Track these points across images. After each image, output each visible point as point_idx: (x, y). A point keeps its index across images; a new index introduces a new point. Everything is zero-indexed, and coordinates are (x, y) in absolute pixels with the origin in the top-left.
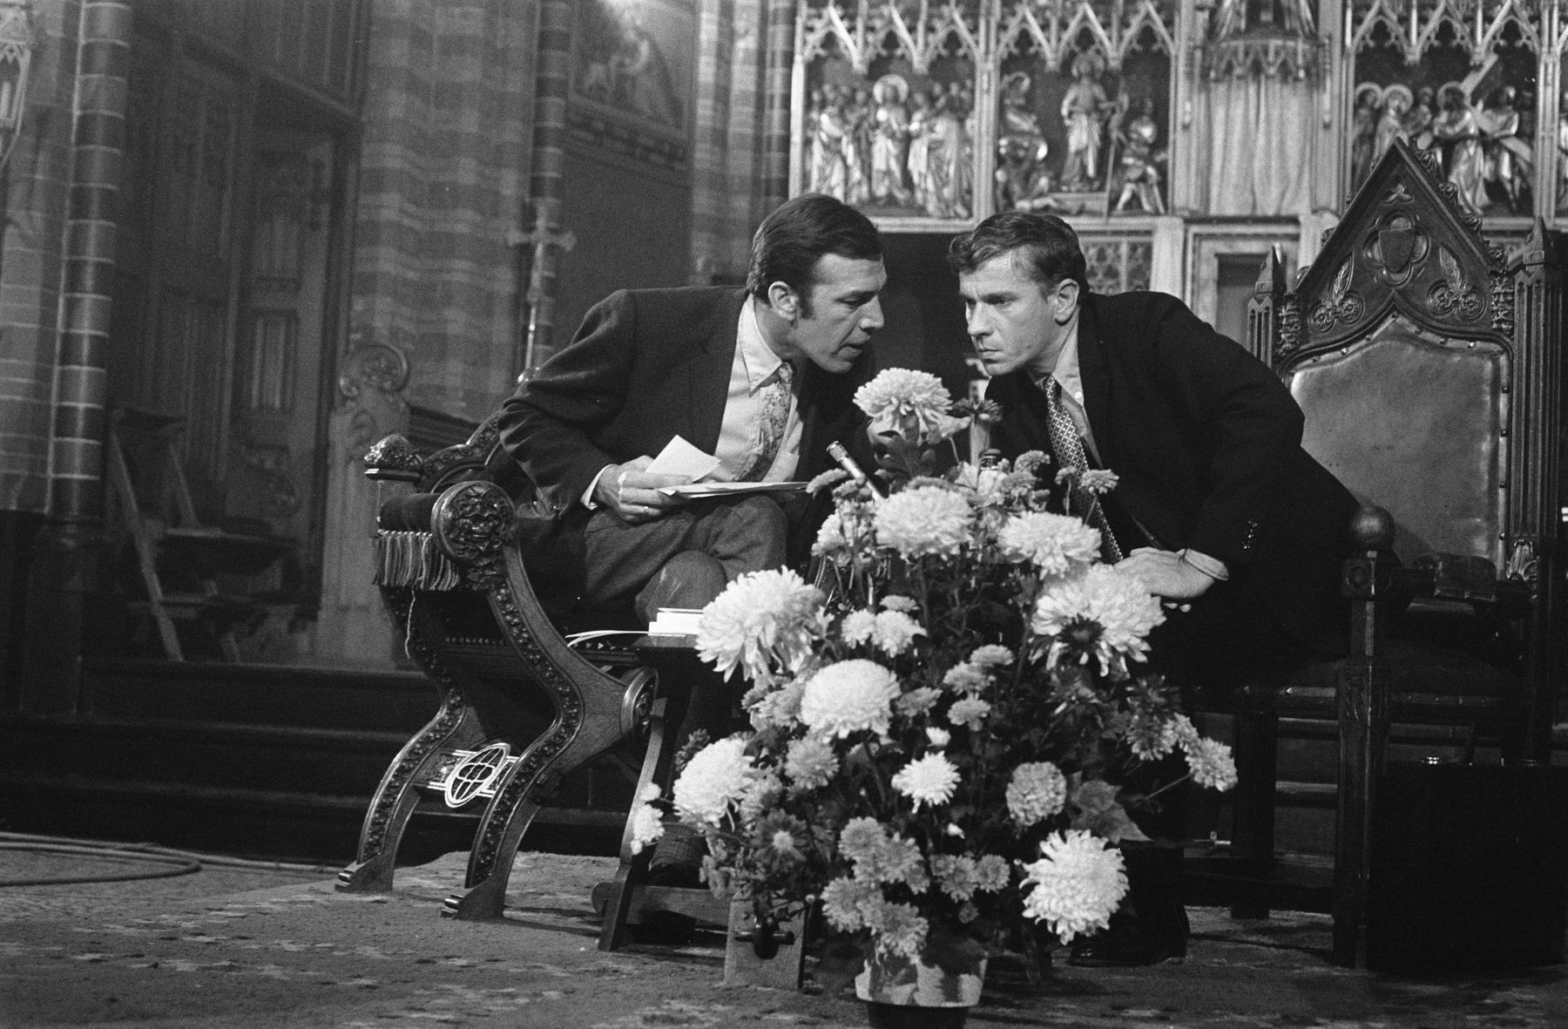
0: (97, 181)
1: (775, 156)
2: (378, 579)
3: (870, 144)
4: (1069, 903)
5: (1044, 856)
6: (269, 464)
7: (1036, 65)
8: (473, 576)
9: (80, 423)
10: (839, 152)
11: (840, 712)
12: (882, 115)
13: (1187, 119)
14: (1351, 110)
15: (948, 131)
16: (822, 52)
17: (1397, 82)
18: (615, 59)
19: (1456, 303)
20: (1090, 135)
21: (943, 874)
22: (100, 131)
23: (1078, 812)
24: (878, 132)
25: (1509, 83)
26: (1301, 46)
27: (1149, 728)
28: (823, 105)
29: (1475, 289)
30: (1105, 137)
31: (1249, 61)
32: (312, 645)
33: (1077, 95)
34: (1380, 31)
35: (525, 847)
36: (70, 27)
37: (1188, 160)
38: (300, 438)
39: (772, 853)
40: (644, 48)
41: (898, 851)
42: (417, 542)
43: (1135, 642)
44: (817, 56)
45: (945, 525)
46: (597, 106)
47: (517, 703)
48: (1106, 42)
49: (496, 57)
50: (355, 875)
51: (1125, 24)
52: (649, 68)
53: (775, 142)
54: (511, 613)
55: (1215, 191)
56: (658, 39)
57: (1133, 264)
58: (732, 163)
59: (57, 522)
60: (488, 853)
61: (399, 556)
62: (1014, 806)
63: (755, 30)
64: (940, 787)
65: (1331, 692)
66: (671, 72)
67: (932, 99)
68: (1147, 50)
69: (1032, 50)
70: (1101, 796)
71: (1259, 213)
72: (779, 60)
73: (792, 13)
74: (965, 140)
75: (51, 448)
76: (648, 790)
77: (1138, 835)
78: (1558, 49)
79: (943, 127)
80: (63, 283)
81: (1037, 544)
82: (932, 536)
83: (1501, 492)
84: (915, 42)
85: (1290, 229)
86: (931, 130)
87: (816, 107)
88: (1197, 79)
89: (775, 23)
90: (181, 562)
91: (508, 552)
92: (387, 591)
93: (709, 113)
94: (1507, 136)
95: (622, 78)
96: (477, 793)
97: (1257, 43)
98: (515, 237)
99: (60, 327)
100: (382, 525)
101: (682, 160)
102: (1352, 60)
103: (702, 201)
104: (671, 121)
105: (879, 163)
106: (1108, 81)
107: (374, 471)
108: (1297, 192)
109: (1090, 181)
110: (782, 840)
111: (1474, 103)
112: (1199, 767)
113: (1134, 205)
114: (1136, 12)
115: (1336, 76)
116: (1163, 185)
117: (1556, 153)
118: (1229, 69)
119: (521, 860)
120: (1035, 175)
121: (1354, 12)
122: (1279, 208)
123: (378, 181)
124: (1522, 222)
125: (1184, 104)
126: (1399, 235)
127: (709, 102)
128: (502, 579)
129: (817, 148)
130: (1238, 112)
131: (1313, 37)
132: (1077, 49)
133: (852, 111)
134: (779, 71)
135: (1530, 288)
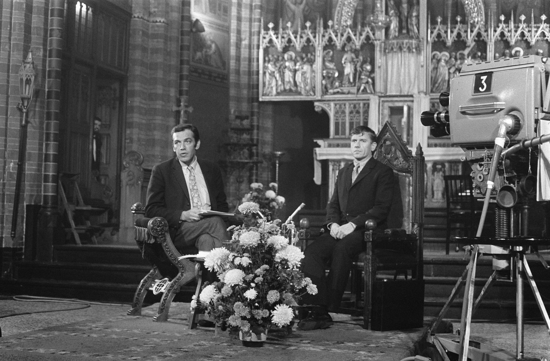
0: (53, 110)
2: (136, 239)
3: (284, 73)
7: (334, 47)
8: (158, 240)
9: (51, 179)
10: (274, 76)
13: (380, 65)
16: (268, 45)
17: (445, 51)
18: (204, 50)
20: (351, 69)
22: (53, 95)
23: (284, 300)
24: (286, 69)
25: (480, 51)
28: (269, 61)
30: (356, 70)
31: (398, 46)
32: (118, 239)
33: (347, 56)
34: (439, 36)
35: (175, 301)
36: (44, 66)
38: (112, 172)
39: (218, 310)
40: (213, 46)
41: (244, 309)
42: (144, 230)
43: (297, 262)
44: (267, 46)
46: (199, 65)
47: (169, 270)
48: (355, 40)
49: (168, 53)
51: (361, 35)
52: (214, 53)
53: (255, 73)
56: (217, 43)
57: (365, 109)
59: (45, 207)
61: (140, 233)
62: (268, 299)
63: (248, 38)
65: (363, 264)
66: (222, 54)
67: (302, 59)
68: (368, 42)
69: (333, 43)
71: (402, 94)
72: (255, 47)
73: (259, 33)
74: (313, 71)
75: (43, 186)
78: (493, 41)
79: (306, 67)
80: (44, 139)
83: (411, 211)
85: (411, 99)
86: (302, 68)
89: (254, 35)
90: (79, 217)
91: (166, 234)
92: (138, 241)
93: (234, 64)
95: (206, 56)
96: (161, 291)
97: (400, 41)
98: (175, 108)
100: (136, 225)
101: (226, 79)
102: (431, 44)
103: (232, 92)
104: (222, 68)
105: (287, 79)
106: (356, 52)
107: (134, 212)
108: (414, 85)
109: (351, 83)
110: (220, 307)
111: (468, 57)
114: (364, 31)
116: (374, 84)
118: (392, 49)
120: (334, 82)
122: (408, 92)
123: (133, 94)
125: (379, 59)
126: (388, 145)
127: (234, 61)
129: (267, 75)
130: (395, 62)
132: (346, 42)
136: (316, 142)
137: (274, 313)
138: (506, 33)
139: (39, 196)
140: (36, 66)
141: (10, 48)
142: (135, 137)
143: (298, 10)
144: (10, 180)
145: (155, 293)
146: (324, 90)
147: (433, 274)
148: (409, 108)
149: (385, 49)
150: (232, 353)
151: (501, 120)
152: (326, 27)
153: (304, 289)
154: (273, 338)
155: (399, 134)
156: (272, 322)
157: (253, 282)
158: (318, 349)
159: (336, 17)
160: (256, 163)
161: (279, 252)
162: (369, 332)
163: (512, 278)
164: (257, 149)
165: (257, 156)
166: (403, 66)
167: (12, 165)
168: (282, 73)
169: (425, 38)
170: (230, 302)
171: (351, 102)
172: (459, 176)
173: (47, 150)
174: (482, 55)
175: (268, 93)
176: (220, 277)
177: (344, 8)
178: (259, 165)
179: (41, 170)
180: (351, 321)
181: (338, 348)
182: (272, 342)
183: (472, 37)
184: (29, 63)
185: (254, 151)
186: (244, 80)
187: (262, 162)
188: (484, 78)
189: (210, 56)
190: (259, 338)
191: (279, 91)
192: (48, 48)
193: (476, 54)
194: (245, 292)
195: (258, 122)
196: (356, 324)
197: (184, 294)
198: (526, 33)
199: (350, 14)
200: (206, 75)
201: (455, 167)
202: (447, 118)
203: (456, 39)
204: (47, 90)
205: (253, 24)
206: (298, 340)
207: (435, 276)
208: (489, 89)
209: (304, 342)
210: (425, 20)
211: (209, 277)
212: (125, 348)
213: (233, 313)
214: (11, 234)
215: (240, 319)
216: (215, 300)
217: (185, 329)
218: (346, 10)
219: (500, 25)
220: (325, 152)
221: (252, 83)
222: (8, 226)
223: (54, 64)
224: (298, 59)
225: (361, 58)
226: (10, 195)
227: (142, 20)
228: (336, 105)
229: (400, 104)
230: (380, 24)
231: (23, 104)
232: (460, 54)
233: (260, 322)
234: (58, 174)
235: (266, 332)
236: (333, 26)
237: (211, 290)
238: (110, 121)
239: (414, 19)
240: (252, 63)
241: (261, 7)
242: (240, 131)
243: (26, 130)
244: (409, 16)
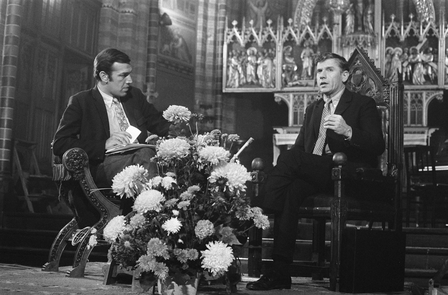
0: (9, 75)
1: (219, 71)
3: (246, 67)
4: (214, 263)
5: (208, 249)
7: (294, 44)
8: (75, 176)
11: (144, 205)
12: (249, 59)
14: (384, 55)
15: (268, 63)
16: (232, 41)
18: (172, 43)
19: (374, 94)
20: (309, 64)
21: (178, 255)
22: (10, 60)
23: (221, 236)
24: (248, 63)
25: (431, 46)
26: (369, 36)
27: (243, 210)
28: (232, 56)
29: (379, 90)
33: (306, 52)
34: (393, 32)
40: (180, 40)
43: (241, 185)
44: (231, 42)
45: (178, 149)
48: (313, 36)
51: (319, 31)
52: (182, 46)
53: (219, 67)
54: (86, 187)
56: (184, 37)
58: (207, 73)
60: (79, 258)
63: (213, 35)
64: (175, 227)
65: (329, 209)
66: (189, 48)
67: (264, 54)
69: (292, 39)
70: (228, 231)
72: (220, 44)
73: (224, 30)
74: (273, 65)
78: (444, 36)
79: (267, 62)
81: (208, 155)
82: (174, 152)
84: (259, 38)
86: (263, 63)
87: (230, 57)
88: (339, 47)
89: (219, 33)
90: (34, 184)
91: (85, 169)
94: (430, 62)
95: (174, 49)
97: (356, 36)
101: (191, 72)
102: (385, 41)
103: (198, 84)
104: (189, 61)
105: (249, 72)
106: (314, 48)
109: (309, 77)
111: (420, 52)
112: (257, 222)
115: (380, 45)
117: (444, 66)
118: (348, 44)
120: (293, 75)
124: (435, 87)
126: (357, 75)
129: (231, 68)
131: (373, 34)
132: (305, 39)
133: (241, 58)
134: (220, 46)
135: (394, 89)
136: (276, 130)
143: (260, 12)
145: (73, 244)
146: (284, 83)
152: (286, 24)
153: (251, 221)
156: (203, 267)
157: (176, 208)
159: (295, 17)
161: (216, 170)
168: (244, 67)
171: (309, 93)
174: (433, 50)
175: (231, 85)
177: (303, 9)
189: (177, 49)
191: (241, 83)
192: (7, 15)
195: (222, 113)
196: (320, 287)
199: (308, 14)
200: (172, 66)
203: (409, 35)
204: (3, 56)
205: (218, 22)
210: (380, 18)
215: (154, 261)
218: (306, 11)
220: (284, 138)
221: (216, 77)
225: (319, 53)
227: (111, 9)
228: (294, 96)
230: (339, 8)
235: (196, 284)
236: (292, 24)
237: (119, 221)
239: (369, 16)
240: (217, 58)
241: (226, 7)
244: (365, 13)
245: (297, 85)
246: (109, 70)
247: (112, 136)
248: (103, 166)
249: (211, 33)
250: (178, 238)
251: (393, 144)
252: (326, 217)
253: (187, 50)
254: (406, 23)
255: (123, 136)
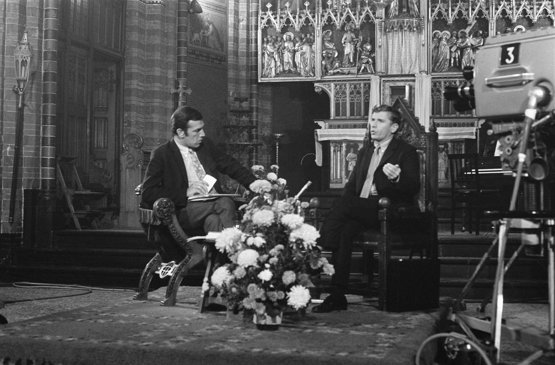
0: (50, 92)
1: (254, 58)
2: (140, 221)
3: (283, 54)
6: (101, 166)
8: (164, 222)
9: (49, 163)
12: (286, 45)
15: (307, 49)
18: (202, 31)
20: (351, 49)
23: (300, 281)
25: (481, 30)
28: (268, 42)
30: (356, 49)
33: (347, 36)
34: (440, 14)
35: (181, 285)
36: (40, 47)
37: (381, 57)
39: (232, 293)
40: (211, 27)
41: (259, 291)
42: (150, 212)
43: (313, 242)
46: (196, 46)
49: (165, 35)
50: (138, 296)
52: (212, 33)
54: (174, 230)
55: (389, 67)
59: (44, 192)
61: (145, 215)
63: (246, 19)
65: (377, 243)
66: (220, 35)
67: (301, 39)
73: (257, 13)
74: (312, 52)
76: (206, 279)
77: (312, 285)
78: (495, 19)
79: (306, 48)
90: (78, 201)
91: (172, 215)
95: (204, 37)
96: (167, 274)
98: (173, 91)
99: (41, 135)
100: (140, 207)
101: (224, 61)
103: (231, 74)
105: (286, 60)
106: (356, 31)
107: (138, 193)
109: (352, 63)
110: (234, 290)
111: (469, 36)
113: (365, 71)
114: (364, 10)
116: (374, 64)
118: (393, 28)
119: (180, 288)
121: (432, 8)
123: (130, 76)
125: (380, 39)
128: (171, 222)
129: (266, 55)
134: (253, 32)
137: (290, 294)
138: (508, 11)
139: (37, 181)
140: (32, 47)
141: (5, 29)
142: (133, 120)
144: (7, 165)
147: (443, 254)
148: (411, 88)
149: (385, 29)
150: (248, 337)
151: (530, 92)
153: (321, 269)
154: (287, 320)
155: (412, 110)
156: (288, 304)
158: (337, 331)
160: (256, 146)
161: (294, 231)
162: (385, 313)
163: (542, 252)
164: (257, 131)
165: (257, 138)
166: (403, 45)
167: (9, 149)
169: (426, 16)
170: (244, 284)
172: (478, 151)
173: (44, 133)
174: (483, 33)
176: (232, 258)
178: (259, 147)
179: (39, 154)
180: (364, 302)
181: (357, 330)
182: (286, 325)
183: (473, 15)
184: (24, 44)
185: (254, 133)
186: (243, 61)
187: (262, 145)
188: (511, 50)
190: (274, 321)
193: (477, 32)
194: (259, 273)
197: (193, 278)
198: (528, 11)
200: (202, 56)
201: (458, 147)
202: (472, 91)
204: (43, 72)
206: (313, 322)
207: (444, 256)
208: (516, 60)
209: (320, 324)
211: (222, 258)
212: (134, 334)
213: (247, 295)
214: (10, 220)
215: (254, 302)
216: (227, 282)
217: (195, 313)
219: (501, 2)
222: (6, 212)
223: (50, 46)
224: (297, 39)
226: (7, 179)
229: (402, 84)
231: (19, 86)
232: (461, 32)
233: (276, 304)
234: (56, 156)
236: (332, 6)
238: (107, 104)
242: (240, 113)
243: (23, 114)
245: (338, 73)
246: (185, 128)
247: (192, 185)
248: (186, 211)
249: (243, 16)
250: (270, 284)
251: (429, 184)
252: (375, 248)
253: (218, 36)
254: (454, 4)
255: (202, 185)
